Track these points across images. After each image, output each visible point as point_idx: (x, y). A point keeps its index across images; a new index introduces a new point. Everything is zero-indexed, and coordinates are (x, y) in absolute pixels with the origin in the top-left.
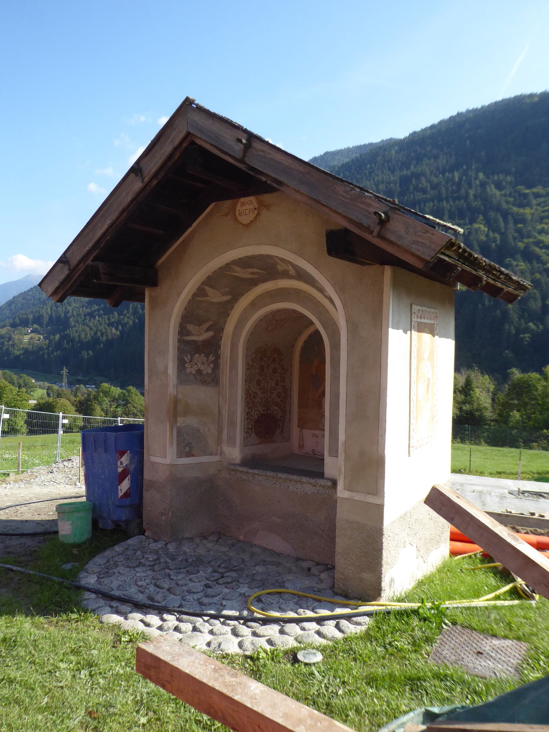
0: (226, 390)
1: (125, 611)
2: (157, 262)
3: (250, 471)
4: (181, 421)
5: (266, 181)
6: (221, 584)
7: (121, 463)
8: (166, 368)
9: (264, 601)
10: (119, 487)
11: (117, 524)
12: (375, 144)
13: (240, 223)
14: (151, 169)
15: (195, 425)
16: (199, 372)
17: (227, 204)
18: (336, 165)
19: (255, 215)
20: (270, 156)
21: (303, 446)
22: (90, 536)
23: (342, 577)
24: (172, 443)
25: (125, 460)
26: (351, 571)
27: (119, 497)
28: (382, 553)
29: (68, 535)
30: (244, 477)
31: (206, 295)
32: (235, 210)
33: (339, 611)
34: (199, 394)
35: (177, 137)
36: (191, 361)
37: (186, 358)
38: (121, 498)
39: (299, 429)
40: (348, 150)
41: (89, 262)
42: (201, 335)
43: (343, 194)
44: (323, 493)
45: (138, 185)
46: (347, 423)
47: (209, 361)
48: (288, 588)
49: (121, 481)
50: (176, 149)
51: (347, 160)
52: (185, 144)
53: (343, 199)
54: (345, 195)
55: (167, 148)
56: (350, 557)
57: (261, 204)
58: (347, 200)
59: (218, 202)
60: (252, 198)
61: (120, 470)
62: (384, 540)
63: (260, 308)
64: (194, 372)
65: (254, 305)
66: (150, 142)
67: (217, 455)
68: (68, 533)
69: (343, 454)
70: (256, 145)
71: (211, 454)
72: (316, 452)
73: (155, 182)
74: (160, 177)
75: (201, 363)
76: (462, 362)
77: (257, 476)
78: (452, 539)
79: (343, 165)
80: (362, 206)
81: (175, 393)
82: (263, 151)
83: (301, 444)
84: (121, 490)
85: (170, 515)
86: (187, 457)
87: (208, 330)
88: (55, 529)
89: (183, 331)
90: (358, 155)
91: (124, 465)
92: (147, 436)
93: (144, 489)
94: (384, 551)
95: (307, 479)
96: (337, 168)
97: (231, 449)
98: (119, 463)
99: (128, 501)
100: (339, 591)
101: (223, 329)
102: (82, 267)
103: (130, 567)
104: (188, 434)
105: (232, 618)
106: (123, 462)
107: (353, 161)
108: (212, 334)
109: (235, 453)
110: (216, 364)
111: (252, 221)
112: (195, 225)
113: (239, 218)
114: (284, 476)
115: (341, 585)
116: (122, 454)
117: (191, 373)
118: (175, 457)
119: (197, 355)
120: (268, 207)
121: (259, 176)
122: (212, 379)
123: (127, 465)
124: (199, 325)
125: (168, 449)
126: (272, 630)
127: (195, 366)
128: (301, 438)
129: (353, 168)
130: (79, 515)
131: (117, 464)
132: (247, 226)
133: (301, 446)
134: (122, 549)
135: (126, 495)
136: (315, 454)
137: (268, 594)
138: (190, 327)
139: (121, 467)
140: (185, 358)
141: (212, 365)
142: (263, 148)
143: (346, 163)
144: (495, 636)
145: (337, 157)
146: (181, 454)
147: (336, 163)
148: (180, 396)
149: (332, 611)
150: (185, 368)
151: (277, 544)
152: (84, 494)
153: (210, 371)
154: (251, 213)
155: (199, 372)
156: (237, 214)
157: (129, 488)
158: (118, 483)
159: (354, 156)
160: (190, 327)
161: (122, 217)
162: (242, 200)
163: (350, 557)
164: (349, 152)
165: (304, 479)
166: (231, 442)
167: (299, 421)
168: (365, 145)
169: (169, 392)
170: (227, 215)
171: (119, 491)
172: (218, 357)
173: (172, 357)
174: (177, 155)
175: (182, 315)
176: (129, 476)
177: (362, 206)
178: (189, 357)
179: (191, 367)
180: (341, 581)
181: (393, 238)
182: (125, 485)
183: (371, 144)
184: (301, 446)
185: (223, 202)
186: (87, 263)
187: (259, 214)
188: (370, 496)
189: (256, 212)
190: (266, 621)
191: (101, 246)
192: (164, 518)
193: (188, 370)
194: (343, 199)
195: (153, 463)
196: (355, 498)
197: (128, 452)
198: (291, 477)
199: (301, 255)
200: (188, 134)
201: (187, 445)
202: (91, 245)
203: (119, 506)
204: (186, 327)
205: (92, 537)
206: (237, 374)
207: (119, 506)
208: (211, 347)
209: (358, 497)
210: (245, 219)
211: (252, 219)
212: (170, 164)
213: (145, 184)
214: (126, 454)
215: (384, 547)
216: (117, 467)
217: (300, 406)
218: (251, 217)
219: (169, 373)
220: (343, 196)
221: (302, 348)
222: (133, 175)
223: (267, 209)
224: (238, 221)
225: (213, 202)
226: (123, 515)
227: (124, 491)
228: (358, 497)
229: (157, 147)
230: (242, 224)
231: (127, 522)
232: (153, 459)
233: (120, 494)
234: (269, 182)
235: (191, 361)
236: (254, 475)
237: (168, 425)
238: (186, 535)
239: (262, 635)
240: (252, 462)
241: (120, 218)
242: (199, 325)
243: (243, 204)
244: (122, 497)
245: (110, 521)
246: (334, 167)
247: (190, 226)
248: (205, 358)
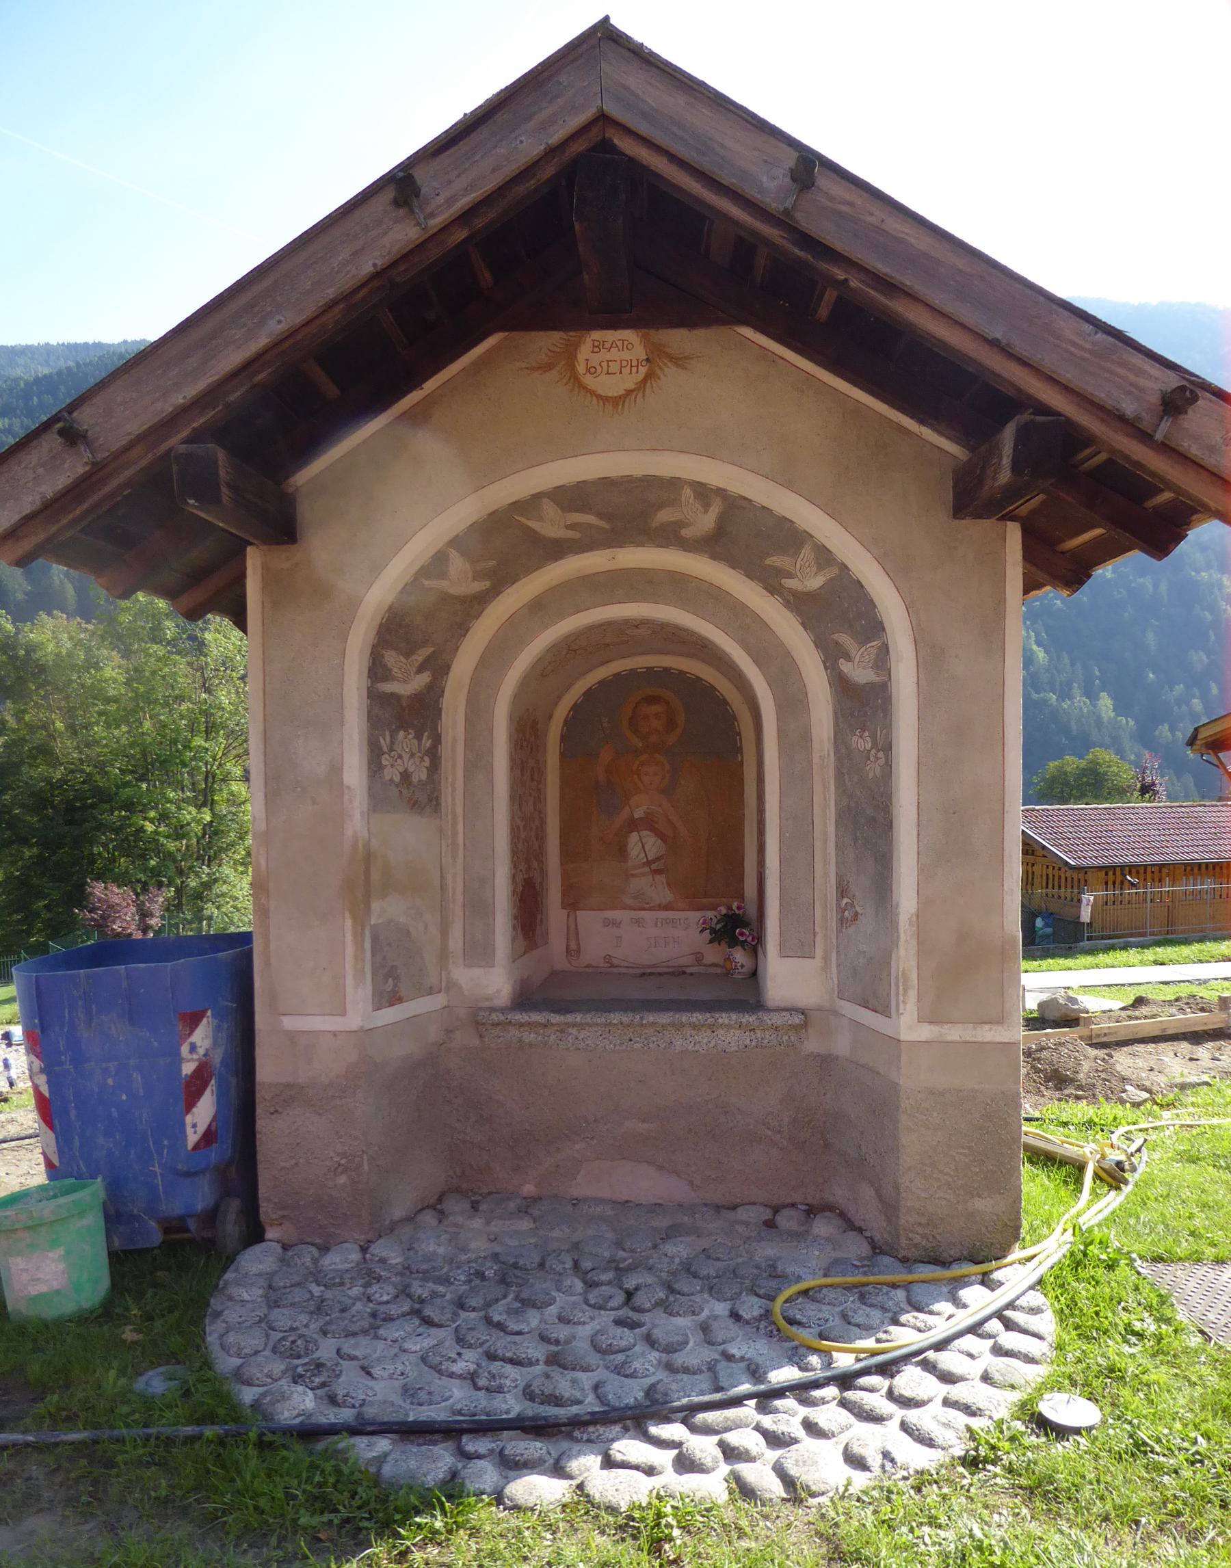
0: (455, 823)
1: (537, 1455)
2: (295, 471)
5: (846, 280)
6: (649, 1311)
7: (193, 1048)
8: (336, 769)
9: (804, 1320)
10: (189, 1119)
11: (173, 1226)
12: (110, 345)
13: (593, 393)
14: (449, 197)
15: (402, 919)
17: (545, 342)
18: (21, 378)
19: (641, 376)
20: (870, 219)
21: (578, 951)
22: (105, 1283)
23: (923, 1221)
24: (359, 974)
25: (203, 1037)
26: (944, 1203)
27: (190, 1146)
29: (58, 1292)
30: (530, 1037)
32: (571, 359)
34: (407, 836)
35: (562, 121)
36: (391, 750)
38: (194, 1148)
39: (565, 912)
40: (47, 351)
41: (175, 441)
42: (407, 686)
43: (1072, 337)
44: (774, 1042)
45: (402, 234)
46: (921, 871)
47: (423, 751)
48: (799, 1279)
49: (191, 1101)
50: (551, 152)
51: (46, 371)
52: (579, 147)
53: (1073, 349)
54: (1080, 342)
55: (524, 146)
56: (941, 1172)
57: (656, 357)
58: (1087, 355)
59: (513, 334)
60: (629, 335)
61: (188, 1068)
63: (562, 615)
64: (397, 779)
65: (540, 608)
66: (459, 116)
68: (56, 1285)
69: (914, 942)
70: (824, 182)
71: (431, 991)
72: (615, 962)
73: (461, 235)
74: (479, 223)
75: (406, 753)
77: (574, 1031)
79: (37, 380)
80: (1123, 372)
81: (366, 833)
82: (852, 205)
83: (573, 945)
84: (194, 1126)
85: (366, 1166)
86: (391, 1005)
87: (420, 670)
89: (377, 671)
90: (71, 363)
91: (201, 1051)
92: (267, 963)
93: (259, 1111)
95: (734, 1017)
96: (22, 385)
97: (477, 972)
98: (185, 1049)
99: (214, 1155)
100: (913, 1253)
101: (449, 667)
102: (143, 460)
103: (354, 1334)
104: (389, 944)
105: (822, 1381)
106: (198, 1044)
107: (59, 373)
108: (428, 680)
109: (495, 982)
111: (629, 392)
112: (431, 385)
113: (588, 380)
114: (665, 1018)
115: (917, 1239)
116: (194, 1020)
118: (370, 1009)
120: (679, 361)
121: (823, 265)
122: (421, 796)
123: (207, 1050)
124: (408, 654)
125: (349, 989)
128: (573, 933)
129: (62, 388)
130: (85, 1222)
131: (179, 1053)
132: (617, 402)
133: (572, 952)
134: (260, 1292)
135: (209, 1137)
136: (613, 966)
139: (192, 1060)
142: (848, 197)
143: (45, 376)
144: (497, 1300)
145: (21, 361)
147: (18, 372)
148: (374, 843)
150: (381, 767)
151: (643, 1183)
153: (424, 776)
154: (626, 371)
156: (581, 369)
157: (215, 1118)
158: (182, 1105)
159: (62, 364)
160: (391, 658)
161: (323, 319)
162: (596, 335)
163: (941, 1172)
164: (48, 355)
165: (724, 1018)
166: (479, 953)
167: (564, 894)
168: (86, 344)
169: (349, 832)
170: (548, 367)
171: (189, 1130)
172: (437, 739)
173: (356, 737)
174: (549, 171)
175: (381, 625)
176: (213, 1082)
177: (1123, 372)
179: (392, 766)
180: (919, 1230)
181: (1195, 451)
182: (203, 1113)
183: (98, 345)
184: (572, 952)
185: (533, 333)
186: (164, 447)
187: (650, 376)
188: (987, 1027)
189: (643, 370)
191: (232, 398)
192: (342, 1179)
194: (1073, 349)
195: (292, 1037)
196: (949, 1038)
197: (209, 1013)
198: (684, 1018)
199: (789, 484)
200: (602, 118)
202: (191, 391)
203: (187, 1174)
204: (383, 656)
205: (114, 1285)
206: (491, 781)
207: (187, 1174)
209: (953, 1033)
210: (611, 385)
211: (632, 386)
212: (520, 190)
213: (427, 235)
214: (205, 1021)
216: (177, 1060)
217: (568, 856)
218: (629, 381)
219: (346, 781)
220: (1074, 344)
221: (566, 722)
222: (790, 159)
223: (679, 366)
224: (582, 387)
225: (501, 329)
226: (199, 1196)
227: (202, 1128)
228: (953, 1033)
229: (475, 137)
230: (599, 397)
231: (211, 1217)
232: (289, 1023)
233: (192, 1138)
234: (854, 283)
235: (391, 750)
236: (562, 1029)
237: (349, 923)
238: (398, 1214)
239: (926, 1398)
240: (524, 999)
241: (318, 322)
242: (408, 654)
243: (598, 347)
244: (197, 1147)
245: (153, 1223)
246: (16, 380)
247: (418, 385)
248: (416, 742)
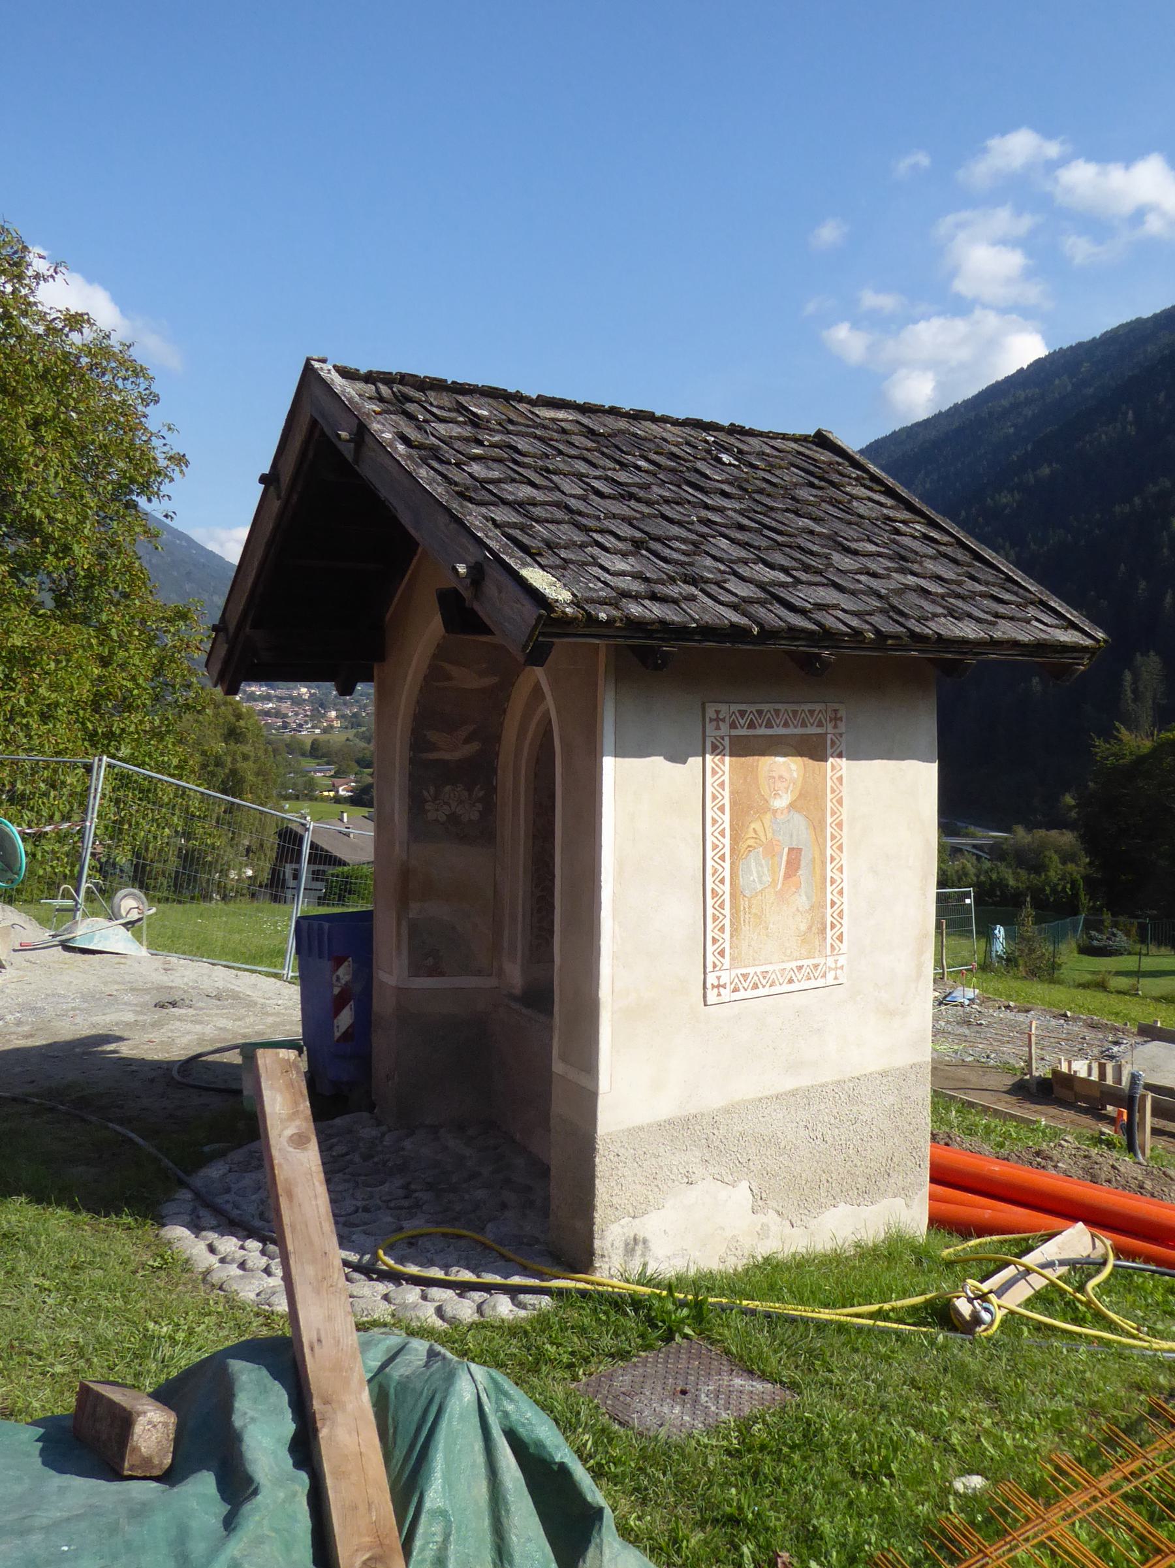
3: (524, 1011)
4: (415, 910)
7: (338, 979)
16: (453, 818)
28: (594, 1185)
31: (449, 678)
33: (516, 1280)
37: (425, 793)
42: (454, 749)
49: (337, 1011)
61: (336, 991)
62: (597, 1160)
64: (443, 818)
67: (490, 975)
71: (479, 973)
73: (295, 497)
76: (956, 808)
78: (934, 1180)
87: (467, 741)
88: (234, 1086)
91: (343, 982)
94: (597, 1181)
110: (489, 808)
116: (339, 962)
117: (437, 820)
119: (448, 788)
122: (482, 832)
126: (412, 1294)
127: (445, 807)
135: (345, 1035)
137: (444, 1235)
138: (432, 736)
140: (425, 793)
141: (479, 806)
146: (416, 969)
149: (881, 1308)
152: (295, 1030)
153: (475, 816)
155: (453, 818)
157: (351, 1026)
160: (432, 736)
178: (432, 790)
182: (345, 1019)
190: (395, 1277)
193: (431, 816)
201: (427, 956)
208: (479, 772)
214: (346, 963)
215: (598, 1174)
227: (343, 1029)
248: (466, 793)
